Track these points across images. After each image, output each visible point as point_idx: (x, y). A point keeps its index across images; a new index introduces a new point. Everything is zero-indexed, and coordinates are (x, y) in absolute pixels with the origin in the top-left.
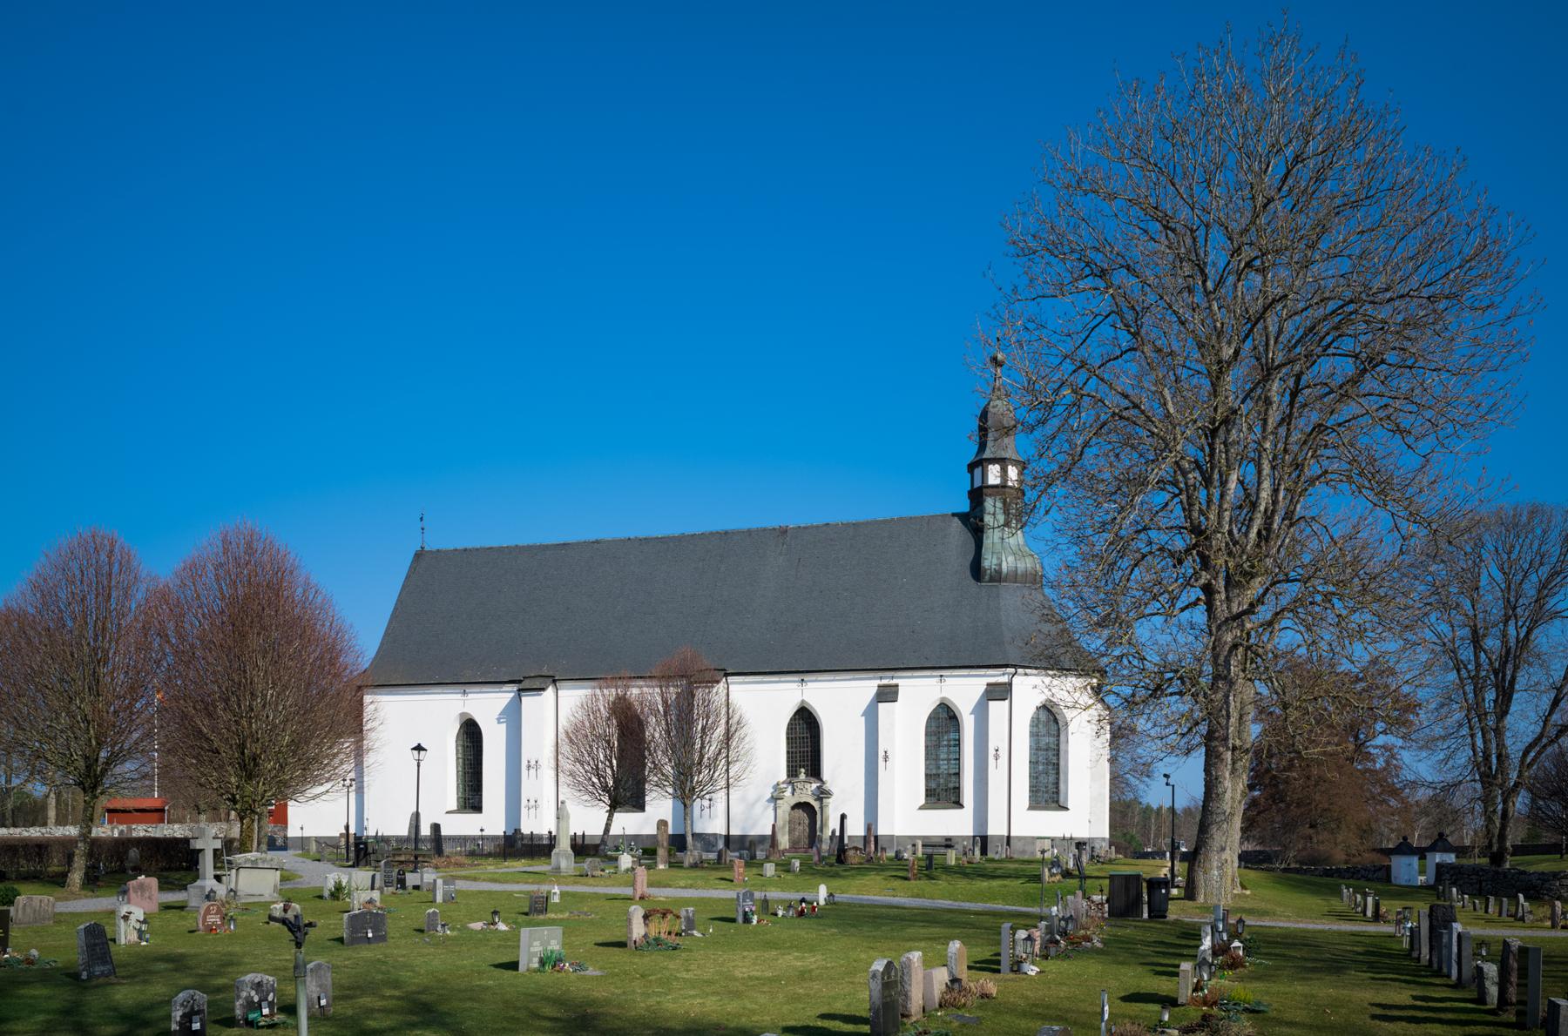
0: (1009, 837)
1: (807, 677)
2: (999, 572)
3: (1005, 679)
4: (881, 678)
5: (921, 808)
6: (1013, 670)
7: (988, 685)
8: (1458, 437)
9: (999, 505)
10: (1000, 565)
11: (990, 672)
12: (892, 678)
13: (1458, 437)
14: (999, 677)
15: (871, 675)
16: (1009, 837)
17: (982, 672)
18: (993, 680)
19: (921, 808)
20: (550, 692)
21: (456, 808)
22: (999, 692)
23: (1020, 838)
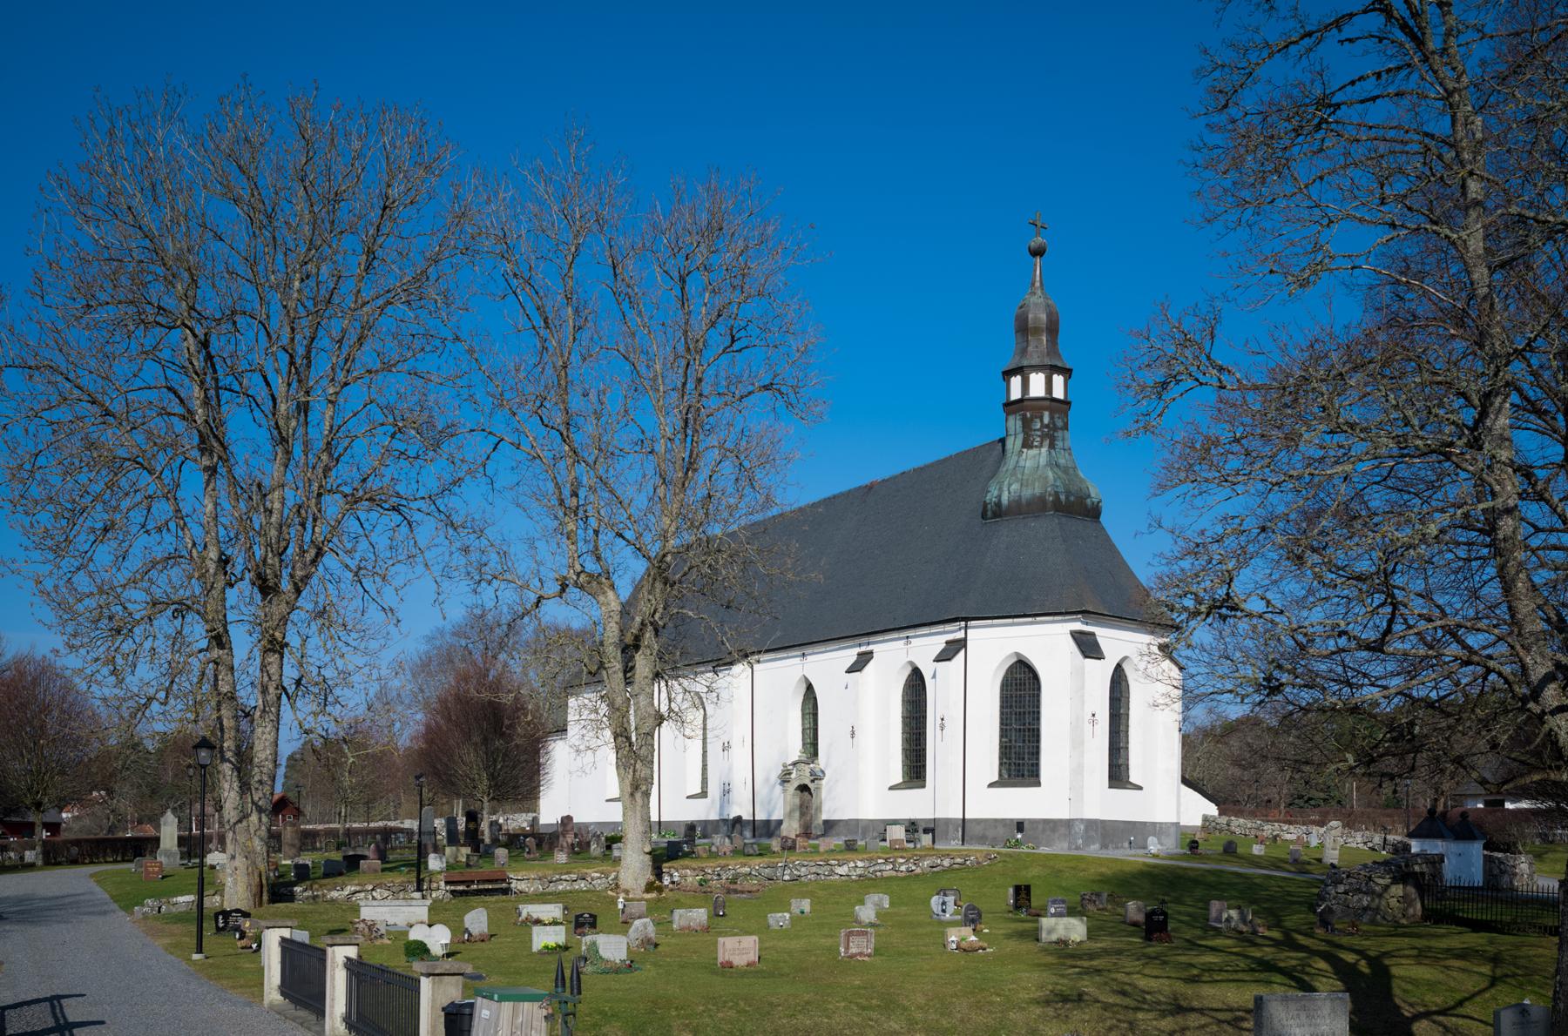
0: (964, 819)
1: (910, 633)
2: (999, 504)
3: (961, 635)
4: (860, 645)
5: (991, 785)
6: (963, 623)
7: (947, 643)
8: (1139, 334)
9: (1019, 423)
10: (999, 497)
11: (948, 627)
12: (869, 644)
13: (1139, 334)
14: (954, 632)
15: (850, 643)
16: (660, 822)
17: (940, 628)
18: (951, 637)
19: (991, 785)
20: (740, 669)
21: (900, 780)
22: (954, 649)
23: (669, 823)
